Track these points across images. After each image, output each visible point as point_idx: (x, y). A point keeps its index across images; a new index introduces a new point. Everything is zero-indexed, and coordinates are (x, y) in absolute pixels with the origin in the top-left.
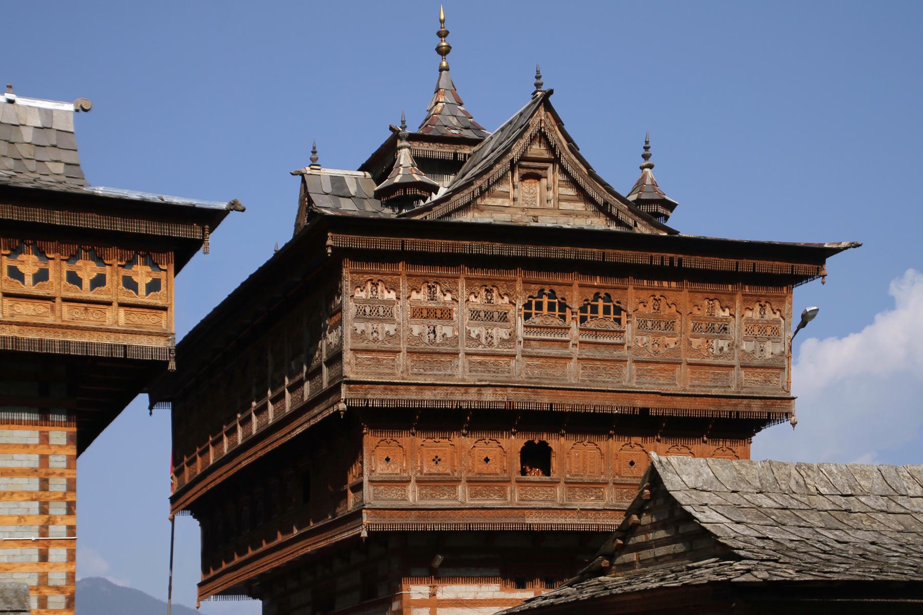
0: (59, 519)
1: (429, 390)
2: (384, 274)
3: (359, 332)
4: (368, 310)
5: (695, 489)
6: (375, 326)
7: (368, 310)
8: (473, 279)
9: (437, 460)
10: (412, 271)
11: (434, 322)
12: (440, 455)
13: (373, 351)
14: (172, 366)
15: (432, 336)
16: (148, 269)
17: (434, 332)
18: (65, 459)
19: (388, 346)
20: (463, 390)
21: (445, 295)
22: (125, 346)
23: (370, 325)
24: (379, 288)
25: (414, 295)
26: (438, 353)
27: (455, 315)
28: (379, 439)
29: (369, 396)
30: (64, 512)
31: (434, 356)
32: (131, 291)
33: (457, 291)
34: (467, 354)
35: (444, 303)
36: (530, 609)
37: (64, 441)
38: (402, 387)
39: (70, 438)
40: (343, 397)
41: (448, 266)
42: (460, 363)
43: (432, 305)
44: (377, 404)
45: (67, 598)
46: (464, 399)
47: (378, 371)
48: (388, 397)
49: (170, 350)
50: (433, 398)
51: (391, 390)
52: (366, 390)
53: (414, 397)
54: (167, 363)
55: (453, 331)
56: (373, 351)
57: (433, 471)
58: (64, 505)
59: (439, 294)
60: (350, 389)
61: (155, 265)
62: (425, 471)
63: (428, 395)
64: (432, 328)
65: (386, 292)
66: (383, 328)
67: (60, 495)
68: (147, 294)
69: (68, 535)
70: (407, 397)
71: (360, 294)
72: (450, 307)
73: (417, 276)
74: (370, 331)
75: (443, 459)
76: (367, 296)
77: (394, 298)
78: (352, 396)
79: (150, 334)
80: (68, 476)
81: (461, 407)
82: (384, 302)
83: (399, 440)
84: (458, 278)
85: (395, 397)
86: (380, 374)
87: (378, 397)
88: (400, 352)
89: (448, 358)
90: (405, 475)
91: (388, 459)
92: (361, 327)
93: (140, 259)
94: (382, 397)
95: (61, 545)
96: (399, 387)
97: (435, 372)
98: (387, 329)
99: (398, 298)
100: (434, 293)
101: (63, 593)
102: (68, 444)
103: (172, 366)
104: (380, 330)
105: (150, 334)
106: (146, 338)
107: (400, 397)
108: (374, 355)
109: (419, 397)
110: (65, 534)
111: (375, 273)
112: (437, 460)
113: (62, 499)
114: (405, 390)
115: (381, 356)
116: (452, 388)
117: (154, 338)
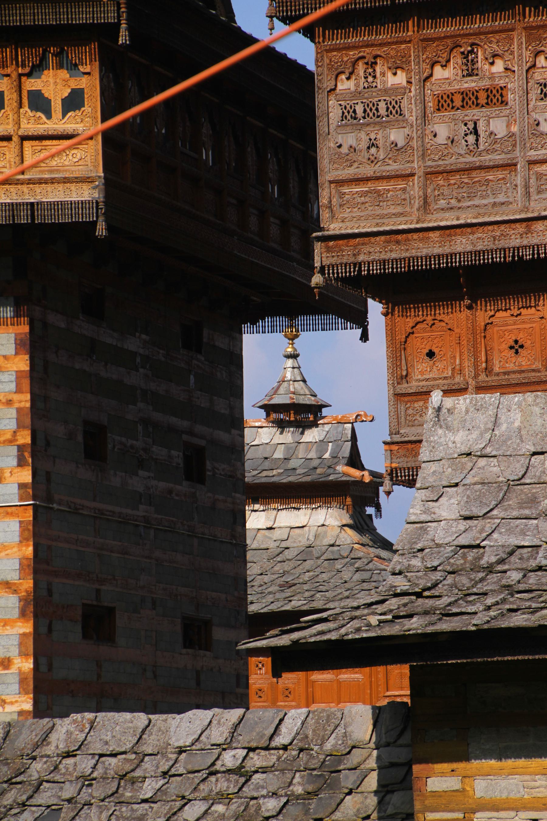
0: (7, 474)
1: (462, 234)
2: (381, 45)
3: (344, 150)
4: (359, 109)
5: (469, 454)
6: (373, 136)
7: (359, 109)
8: (538, 27)
9: (517, 347)
10: (429, 32)
11: (473, 113)
12: (522, 337)
13: (368, 179)
14: (101, 230)
15: (471, 139)
16: (64, 74)
17: (475, 132)
18: (13, 378)
19: (393, 167)
20: (521, 228)
21: (492, 64)
22: (32, 204)
23: (363, 135)
24: (378, 69)
25: (439, 73)
26: (480, 168)
27: (510, 97)
28: (411, 322)
29: (361, 258)
30: (15, 462)
31: (474, 174)
32: (39, 114)
33: (512, 53)
34: (532, 163)
35: (492, 77)
36: (404, 635)
37: (11, 349)
38: (415, 236)
39: (19, 345)
40: (317, 264)
41: (495, 11)
42: (519, 180)
43: (470, 84)
44: (376, 270)
45: (20, 600)
46: (525, 243)
47: (379, 212)
48: (394, 255)
49: (97, 203)
50: (469, 248)
51: (398, 242)
52: (355, 246)
53: (437, 251)
54: (95, 223)
55: (508, 126)
56: (368, 179)
57: (511, 366)
58: (13, 450)
59: (481, 63)
60: (329, 250)
61: (73, 67)
62: (497, 369)
63: (462, 244)
64: (471, 126)
65: (390, 74)
66: (386, 137)
67: (9, 436)
68: (64, 116)
69: (21, 499)
70: (424, 252)
71: (345, 85)
72: (502, 83)
73: (439, 39)
74: (364, 145)
75: (528, 344)
76: (357, 85)
77: (404, 83)
78: (333, 261)
79: (66, 181)
80: (17, 405)
81: (521, 258)
82: (386, 91)
83: (446, 318)
84: (513, 30)
85: (404, 255)
86: (382, 217)
87: (376, 257)
88: (412, 175)
89: (500, 174)
90: (458, 379)
91: (431, 354)
92: (349, 139)
93: (51, 60)
94: (383, 256)
95: (11, 514)
96: (409, 236)
97: (476, 202)
98: (392, 138)
99: (409, 82)
100: (473, 62)
101: (15, 592)
102: (17, 354)
103: (101, 230)
104: (380, 143)
105: (66, 181)
106: (61, 187)
107: (414, 253)
108: (371, 185)
109: (447, 250)
110: (17, 497)
111: (367, 46)
112: (517, 347)
113: (10, 442)
114: (421, 240)
115: (381, 186)
116: (503, 227)
117: (73, 186)
